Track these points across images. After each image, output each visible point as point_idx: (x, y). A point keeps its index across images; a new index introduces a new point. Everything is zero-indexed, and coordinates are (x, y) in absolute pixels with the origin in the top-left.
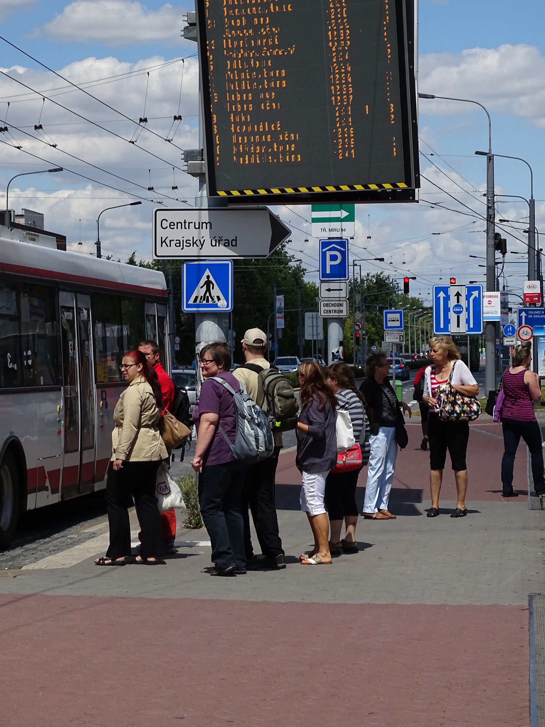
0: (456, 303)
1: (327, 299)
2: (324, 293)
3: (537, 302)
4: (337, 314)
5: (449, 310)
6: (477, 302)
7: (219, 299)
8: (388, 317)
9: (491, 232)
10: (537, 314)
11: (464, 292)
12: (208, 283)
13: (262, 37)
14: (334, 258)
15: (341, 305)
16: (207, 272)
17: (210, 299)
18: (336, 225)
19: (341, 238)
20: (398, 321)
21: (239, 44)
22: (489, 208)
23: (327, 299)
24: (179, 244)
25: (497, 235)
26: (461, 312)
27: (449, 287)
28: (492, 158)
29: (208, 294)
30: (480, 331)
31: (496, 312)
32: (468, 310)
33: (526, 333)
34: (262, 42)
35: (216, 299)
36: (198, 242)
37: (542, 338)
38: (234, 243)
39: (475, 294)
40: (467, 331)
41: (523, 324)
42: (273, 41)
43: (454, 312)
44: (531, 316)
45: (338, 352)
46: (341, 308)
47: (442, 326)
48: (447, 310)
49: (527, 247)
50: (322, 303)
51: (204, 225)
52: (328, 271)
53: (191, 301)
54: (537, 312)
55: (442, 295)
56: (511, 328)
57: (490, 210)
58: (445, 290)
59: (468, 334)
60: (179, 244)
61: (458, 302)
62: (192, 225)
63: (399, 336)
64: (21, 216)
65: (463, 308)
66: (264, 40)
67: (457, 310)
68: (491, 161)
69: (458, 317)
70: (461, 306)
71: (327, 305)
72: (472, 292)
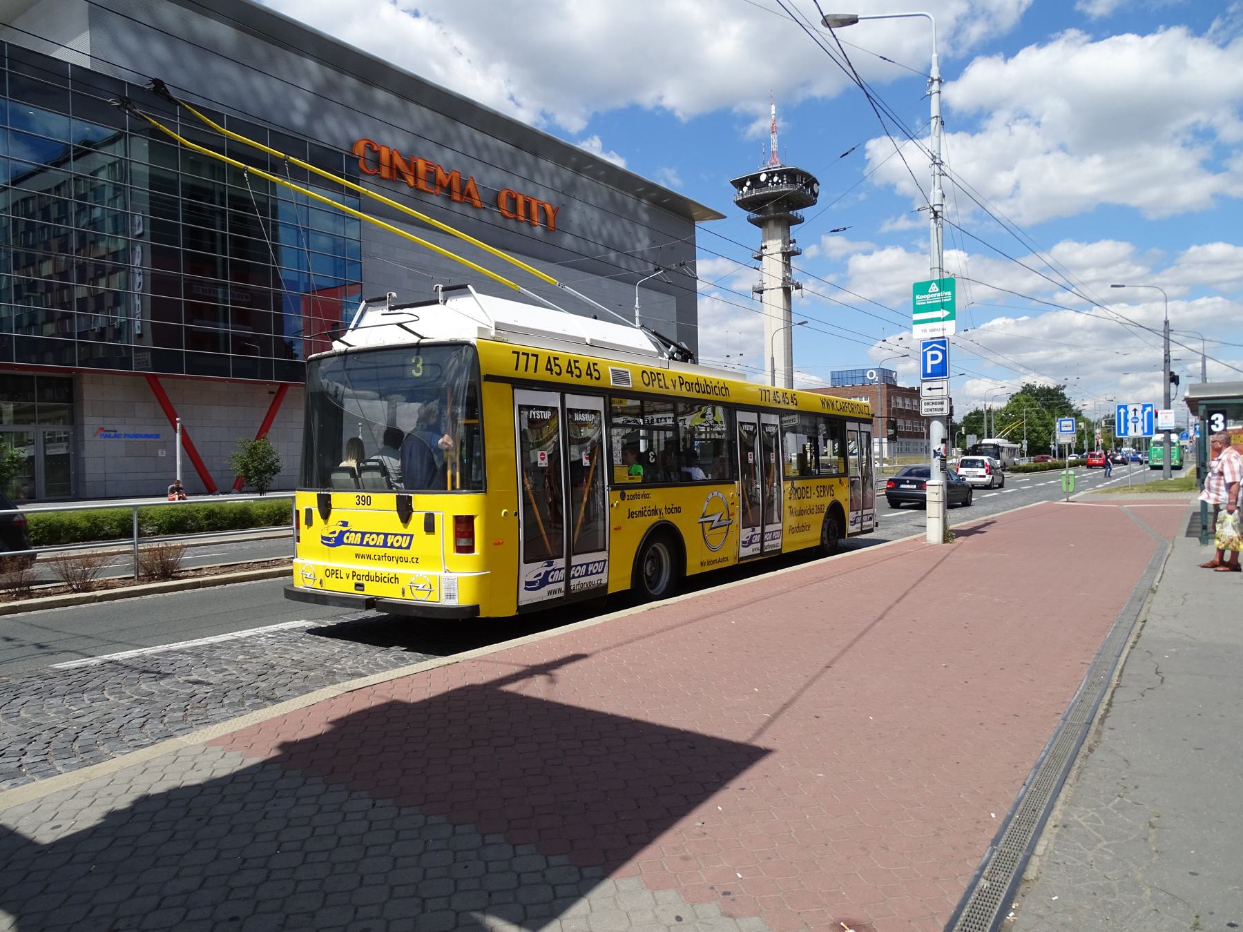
1: (927, 398)
2: (924, 393)
5: (1128, 421)
11: (1140, 408)
14: (934, 357)
18: (938, 325)
19: (943, 337)
22: (1165, 355)
23: (927, 398)
25: (1172, 373)
26: (1133, 418)
31: (1171, 423)
32: (1143, 420)
45: (939, 449)
47: (1122, 432)
48: (1126, 421)
49: (1170, 338)
50: (923, 402)
52: (929, 371)
55: (1122, 411)
58: (1125, 407)
61: (1135, 414)
69: (1135, 426)
70: (1133, 422)
71: (928, 404)
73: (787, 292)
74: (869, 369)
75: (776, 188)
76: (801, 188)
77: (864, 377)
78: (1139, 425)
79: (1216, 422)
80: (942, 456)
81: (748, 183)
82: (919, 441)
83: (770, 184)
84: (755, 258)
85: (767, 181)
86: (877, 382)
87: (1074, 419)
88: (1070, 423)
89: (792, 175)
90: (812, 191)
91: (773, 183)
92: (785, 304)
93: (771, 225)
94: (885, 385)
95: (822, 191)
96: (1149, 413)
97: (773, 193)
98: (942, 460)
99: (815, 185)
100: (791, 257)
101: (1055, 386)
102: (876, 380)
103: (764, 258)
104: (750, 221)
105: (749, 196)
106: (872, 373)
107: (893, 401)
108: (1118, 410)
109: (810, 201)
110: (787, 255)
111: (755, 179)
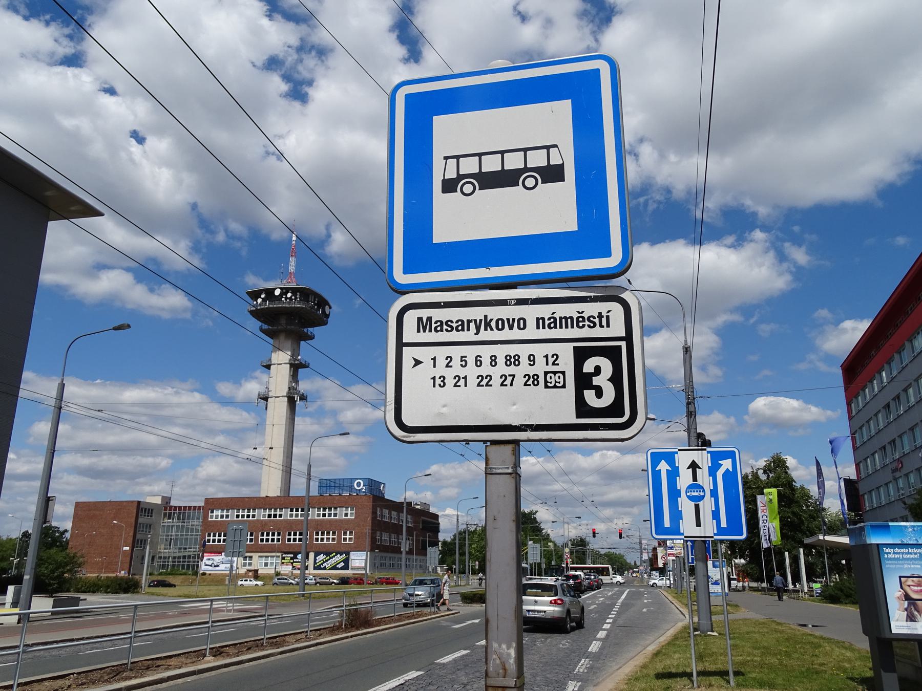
8: (439, 150)
9: (693, 431)
20: (552, 174)
22: (688, 404)
27: (677, 453)
28: (688, 349)
30: (742, 535)
32: (714, 493)
37: (889, 550)
39: (727, 464)
40: (715, 534)
43: (688, 497)
47: (667, 524)
48: (674, 494)
57: (690, 406)
58: (670, 458)
59: (718, 540)
61: (695, 479)
63: (566, 353)
64: (419, 505)
65: (704, 491)
68: (688, 352)
69: (697, 507)
70: (701, 488)
73: (291, 402)
74: (357, 479)
75: (289, 303)
76: (312, 307)
77: (352, 486)
78: (707, 506)
81: (263, 296)
82: (397, 556)
83: (283, 299)
84: (263, 366)
85: (281, 295)
86: (364, 492)
89: (305, 294)
90: (324, 311)
91: (286, 298)
92: (289, 414)
93: (282, 337)
94: (372, 496)
95: (335, 310)
96: (727, 473)
97: (285, 307)
99: (327, 307)
100: (299, 370)
101: (529, 511)
102: (363, 490)
103: (272, 367)
104: (262, 330)
105: (263, 307)
106: (360, 482)
107: (378, 513)
108: (654, 465)
109: (322, 321)
110: (296, 367)
111: (270, 292)
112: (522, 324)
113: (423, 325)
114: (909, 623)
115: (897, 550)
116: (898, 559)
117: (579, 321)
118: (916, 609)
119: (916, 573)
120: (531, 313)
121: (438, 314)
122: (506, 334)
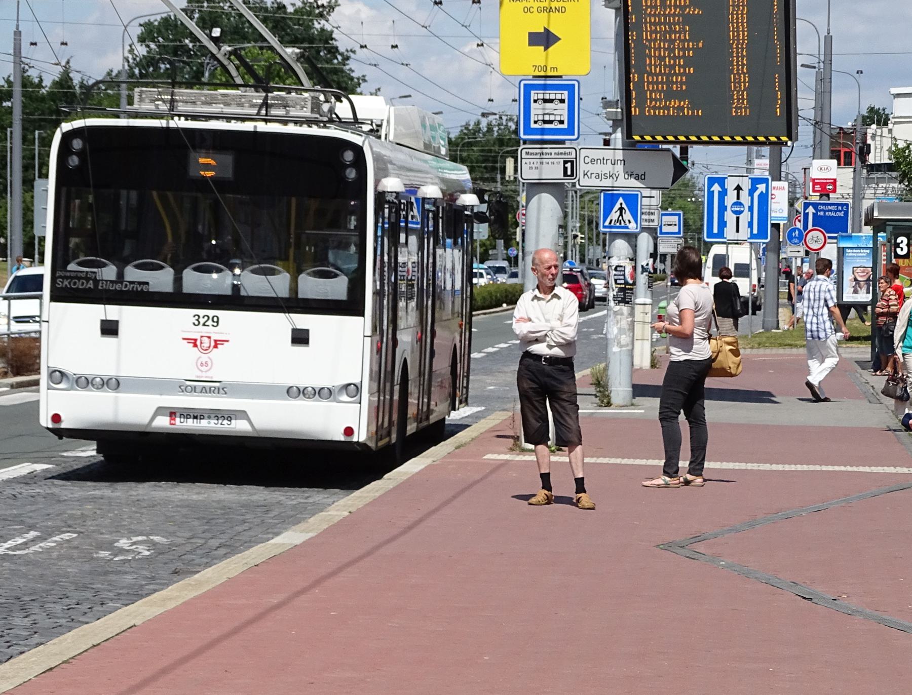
0: (735, 200)
3: (831, 192)
4: (647, 224)
5: (725, 208)
6: (764, 199)
7: (629, 222)
8: (533, 112)
10: (831, 211)
11: (746, 184)
12: (621, 209)
13: (675, 32)
15: (652, 214)
16: (621, 200)
17: (622, 222)
21: (656, 36)
24: (598, 176)
29: (621, 218)
32: (751, 209)
33: (815, 239)
34: (675, 36)
35: (627, 222)
36: (614, 176)
38: (643, 177)
39: (762, 188)
41: (810, 227)
42: (685, 36)
43: (733, 211)
44: (821, 213)
45: (647, 265)
46: (652, 217)
47: (715, 231)
48: (722, 208)
51: (619, 162)
53: (607, 223)
54: (830, 208)
56: (797, 232)
58: (721, 181)
60: (598, 176)
61: (738, 198)
62: (609, 162)
66: (678, 35)
67: (736, 209)
69: (738, 219)
70: (741, 204)
72: (757, 186)
78: (745, 218)
79: (901, 245)
80: (650, 273)
87: (681, 213)
88: (675, 219)
98: (650, 277)
112: (551, 154)
113: (527, 153)
114: (854, 295)
115: (854, 251)
116: (854, 256)
117: (565, 154)
118: (859, 287)
119: (863, 265)
120: (553, 151)
121: (531, 151)
122: (547, 156)
